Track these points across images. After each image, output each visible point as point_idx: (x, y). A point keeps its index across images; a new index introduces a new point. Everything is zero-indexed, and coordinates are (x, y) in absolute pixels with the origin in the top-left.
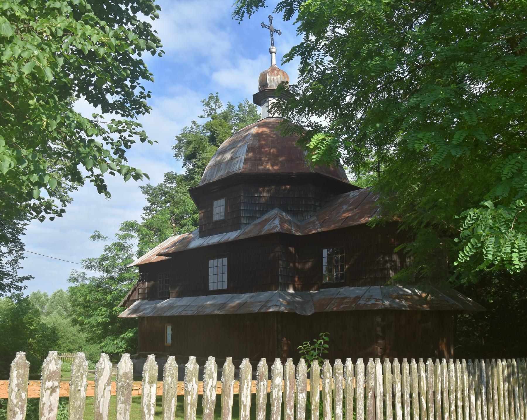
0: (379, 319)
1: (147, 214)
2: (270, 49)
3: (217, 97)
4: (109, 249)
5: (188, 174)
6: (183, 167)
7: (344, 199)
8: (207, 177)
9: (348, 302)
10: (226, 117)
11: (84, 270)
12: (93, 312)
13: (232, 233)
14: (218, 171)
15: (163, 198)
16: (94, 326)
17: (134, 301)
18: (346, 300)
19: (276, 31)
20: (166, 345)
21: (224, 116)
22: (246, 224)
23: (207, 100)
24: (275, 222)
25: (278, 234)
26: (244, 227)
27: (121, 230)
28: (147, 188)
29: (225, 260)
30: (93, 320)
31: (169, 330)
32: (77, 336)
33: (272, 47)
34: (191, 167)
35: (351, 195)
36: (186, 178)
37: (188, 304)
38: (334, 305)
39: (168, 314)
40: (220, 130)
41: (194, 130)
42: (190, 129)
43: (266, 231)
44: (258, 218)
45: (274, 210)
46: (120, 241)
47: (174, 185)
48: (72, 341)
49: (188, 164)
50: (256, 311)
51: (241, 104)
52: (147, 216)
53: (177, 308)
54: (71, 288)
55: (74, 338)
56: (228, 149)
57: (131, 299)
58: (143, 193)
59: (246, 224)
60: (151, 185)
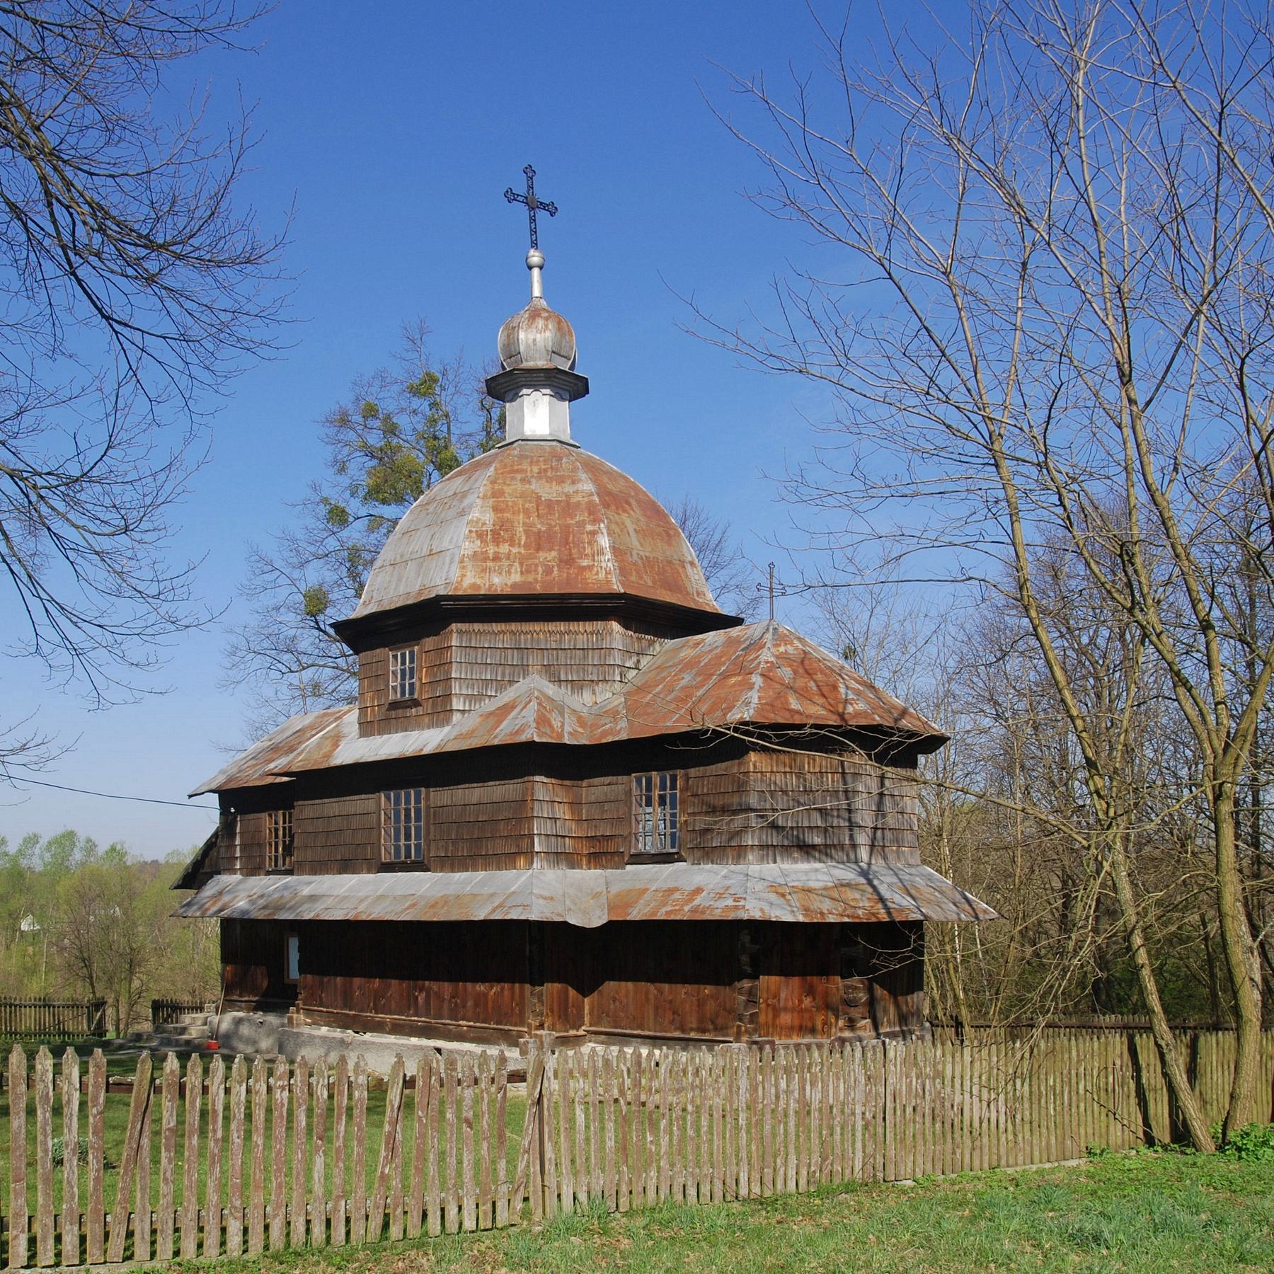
0: (746, 939)
19: (544, 206)
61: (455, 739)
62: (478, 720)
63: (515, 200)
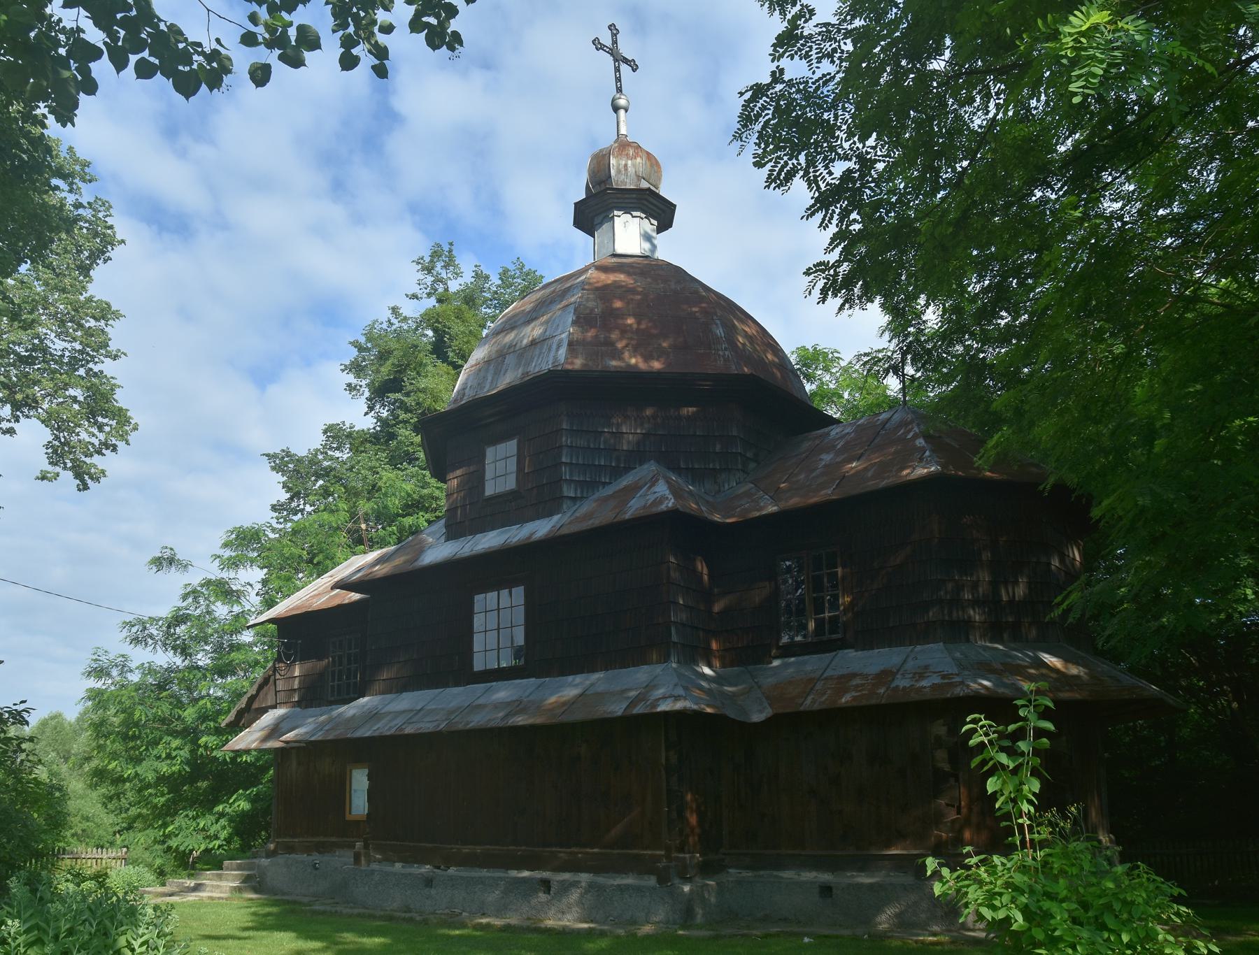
1: (282, 520)
2: (613, 100)
3: (450, 251)
4: (193, 594)
5: (378, 428)
6: (366, 414)
7: (817, 442)
8: (467, 391)
9: (862, 685)
10: (470, 298)
11: (128, 649)
12: (147, 749)
13: (537, 523)
14: (497, 373)
15: (321, 482)
16: (149, 786)
17: (264, 711)
18: (857, 681)
19: (626, 61)
20: (348, 817)
21: (465, 297)
22: (574, 499)
23: (427, 259)
24: (656, 489)
25: (673, 514)
26: (569, 508)
27: (225, 545)
28: (283, 458)
29: (519, 592)
30: (147, 771)
31: (360, 781)
32: (91, 821)
33: (618, 96)
34: (385, 414)
35: (833, 433)
36: (375, 438)
37: (419, 708)
38: (825, 693)
39: (366, 732)
40: (457, 328)
41: (394, 327)
42: (385, 326)
43: (637, 509)
44: (604, 484)
45: (645, 466)
46: (225, 575)
47: (345, 455)
48: (80, 832)
49: (378, 407)
50: (619, 713)
51: (506, 271)
52: (281, 523)
53: (388, 718)
54: (91, 690)
55: (85, 825)
56: (519, 323)
57: (255, 705)
58: (273, 468)
59: (574, 499)
60: (293, 451)
61: (569, 523)
62: (594, 505)
63: (601, 48)
